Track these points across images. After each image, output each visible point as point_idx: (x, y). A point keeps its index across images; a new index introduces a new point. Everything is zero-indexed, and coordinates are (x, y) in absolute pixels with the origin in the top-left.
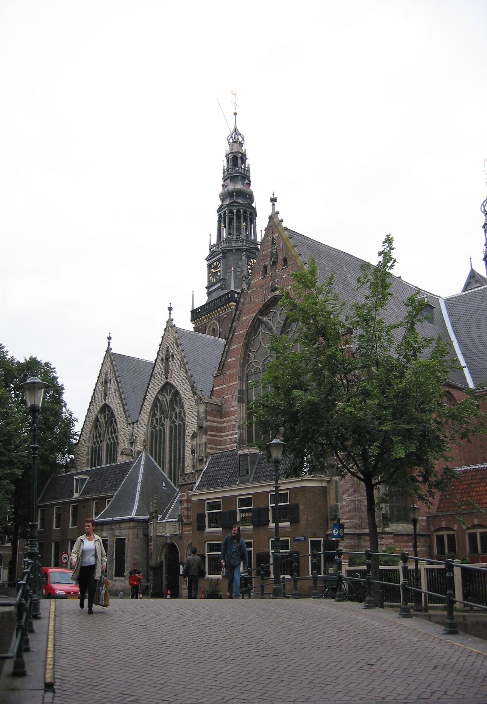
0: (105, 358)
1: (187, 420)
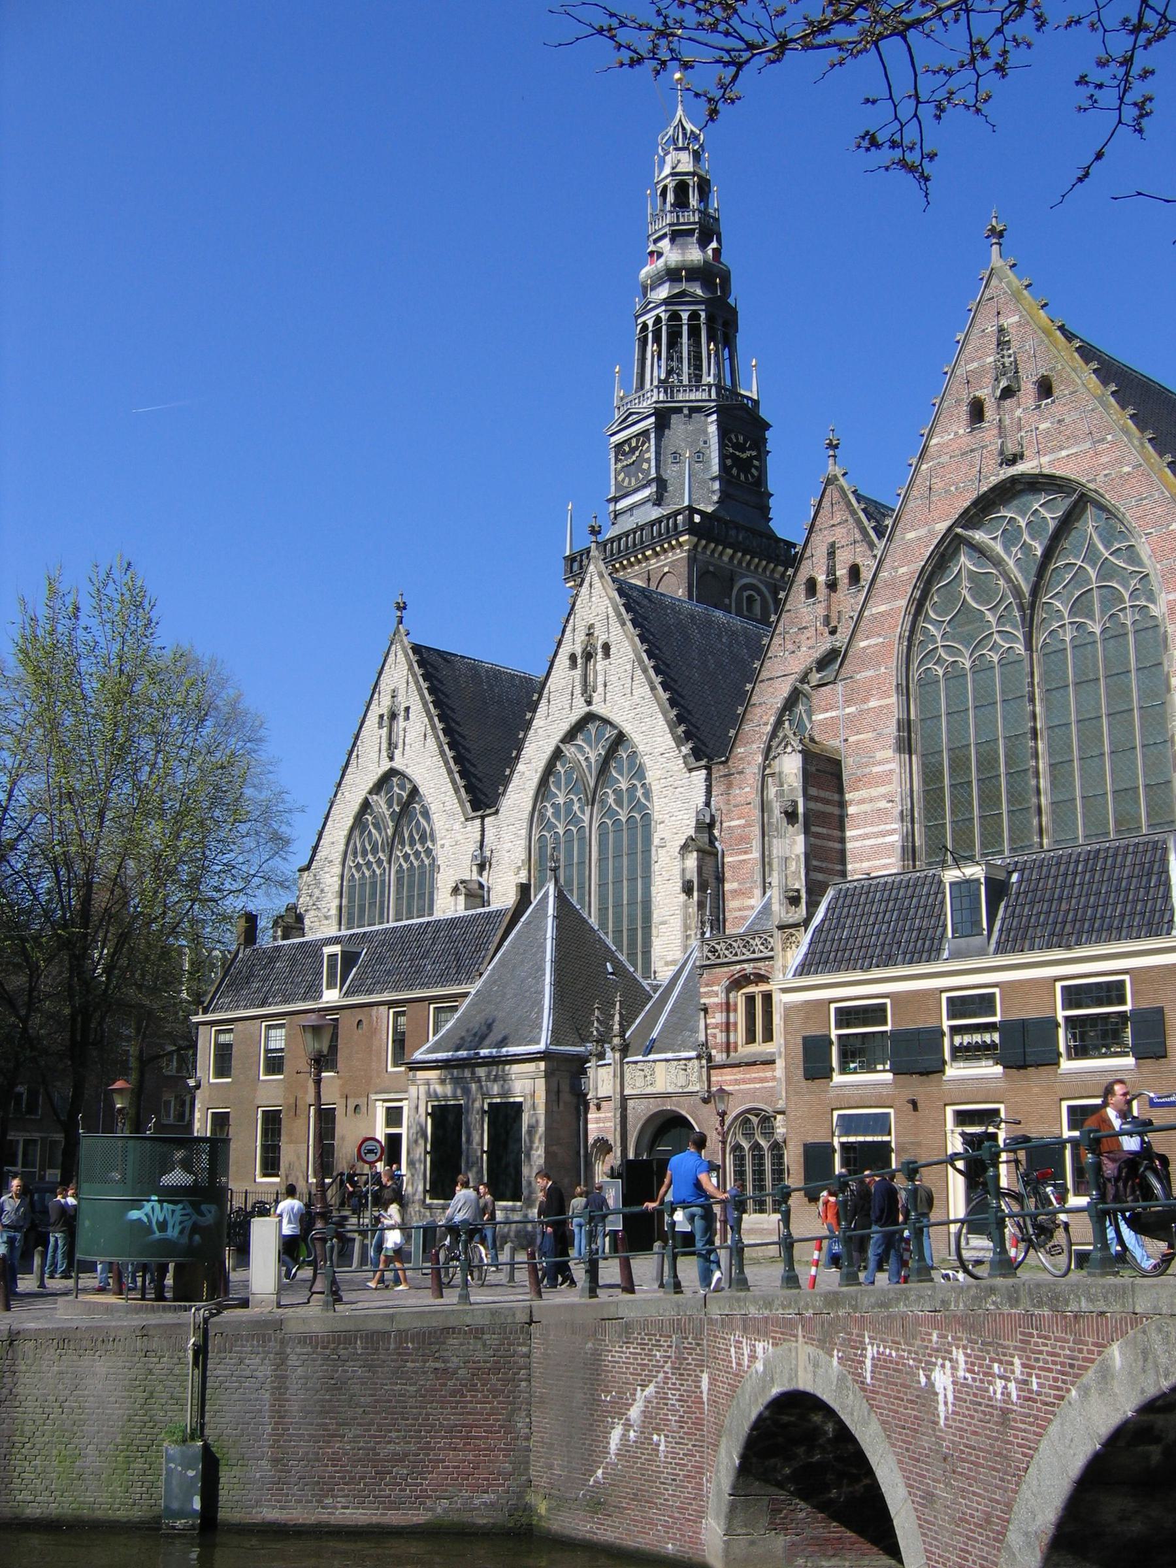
1: (656, 808)
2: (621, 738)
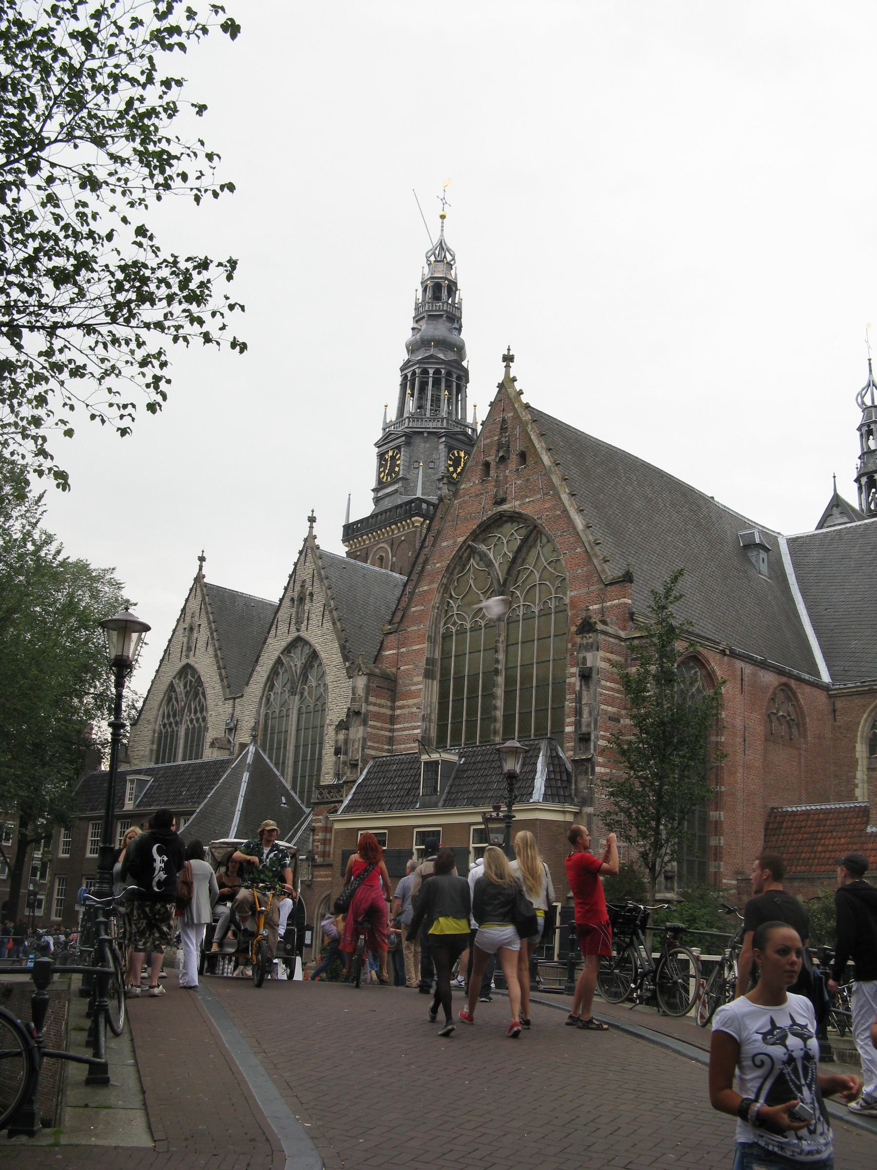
0: (191, 590)
1: (330, 700)
2: (314, 655)
